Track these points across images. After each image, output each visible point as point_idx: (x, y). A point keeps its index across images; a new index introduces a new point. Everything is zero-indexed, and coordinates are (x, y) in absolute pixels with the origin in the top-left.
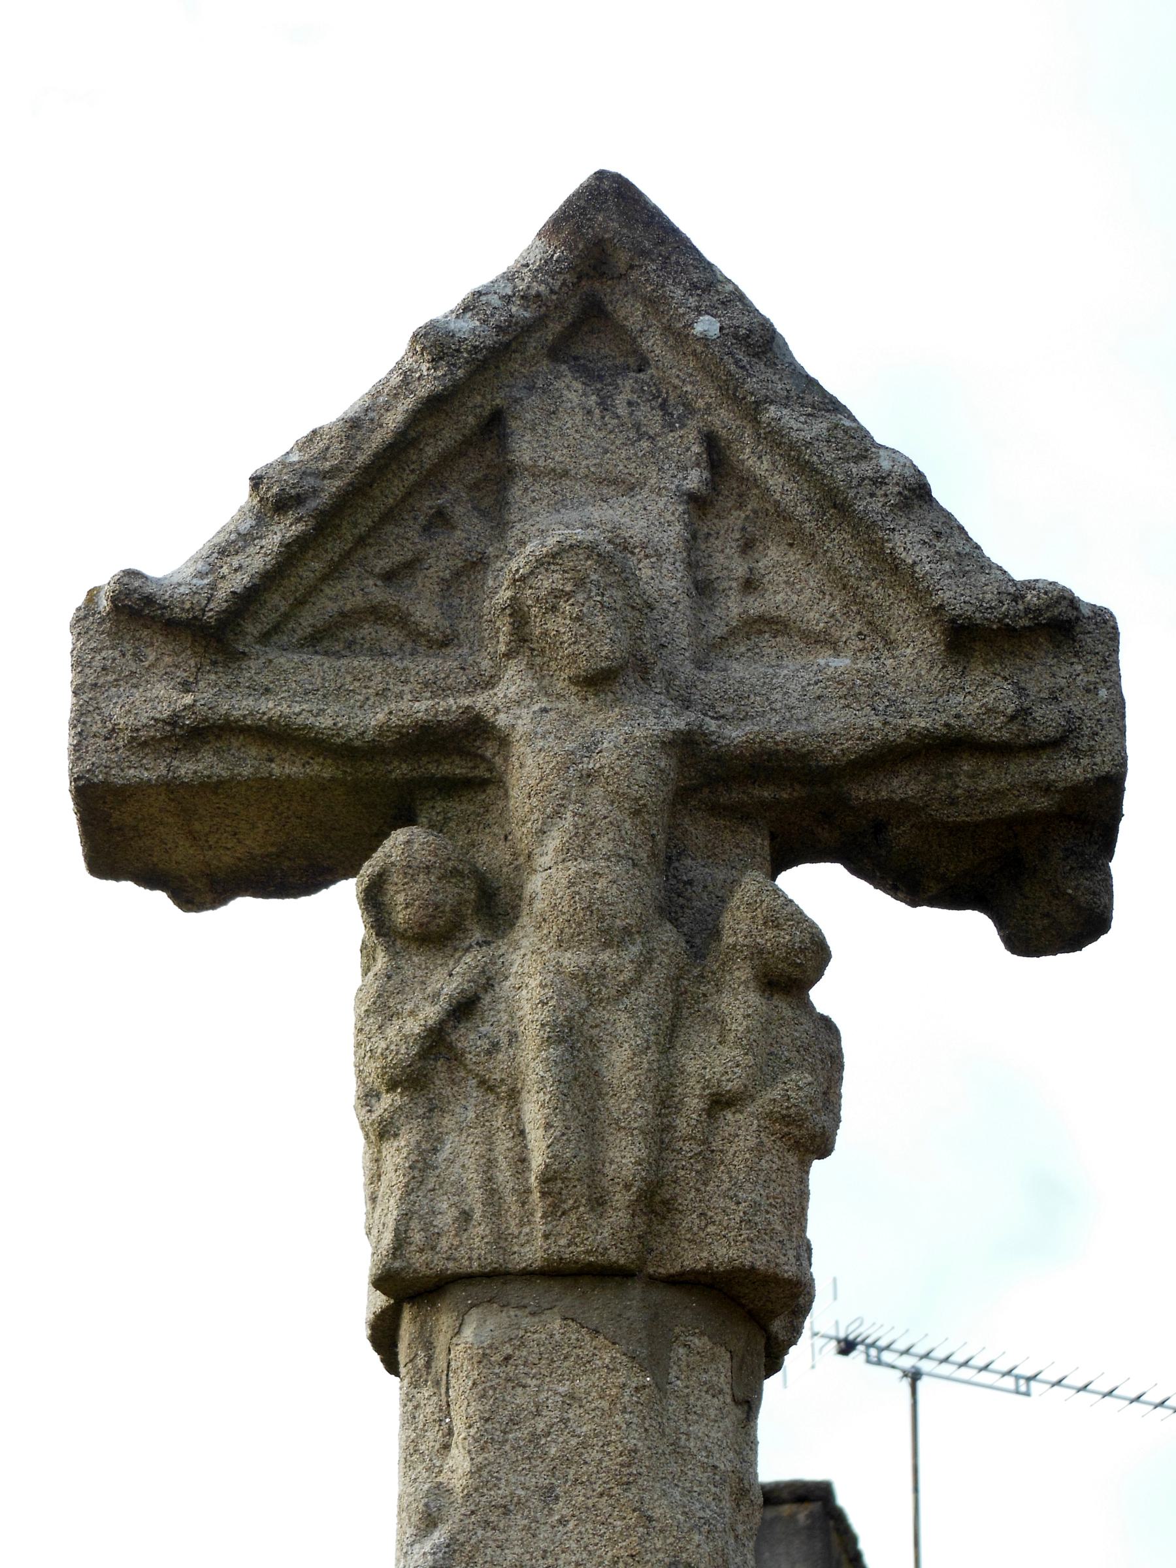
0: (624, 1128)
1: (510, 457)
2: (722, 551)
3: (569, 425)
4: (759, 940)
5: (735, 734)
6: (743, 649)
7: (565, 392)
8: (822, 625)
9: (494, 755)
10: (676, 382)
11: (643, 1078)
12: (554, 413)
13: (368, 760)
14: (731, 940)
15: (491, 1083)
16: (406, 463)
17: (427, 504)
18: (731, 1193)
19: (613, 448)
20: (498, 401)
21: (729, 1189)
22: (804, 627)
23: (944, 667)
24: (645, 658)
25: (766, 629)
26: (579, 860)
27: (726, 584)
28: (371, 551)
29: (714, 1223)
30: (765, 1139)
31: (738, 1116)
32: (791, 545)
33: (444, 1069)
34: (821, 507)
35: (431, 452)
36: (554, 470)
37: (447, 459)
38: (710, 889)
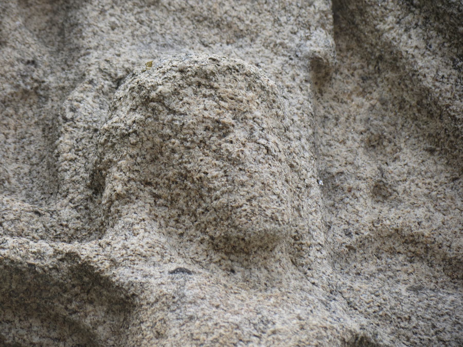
6: (373, 268)
9: (95, 325)
22: (450, 255)
25: (401, 249)
27: (352, 182)
32: (432, 151)
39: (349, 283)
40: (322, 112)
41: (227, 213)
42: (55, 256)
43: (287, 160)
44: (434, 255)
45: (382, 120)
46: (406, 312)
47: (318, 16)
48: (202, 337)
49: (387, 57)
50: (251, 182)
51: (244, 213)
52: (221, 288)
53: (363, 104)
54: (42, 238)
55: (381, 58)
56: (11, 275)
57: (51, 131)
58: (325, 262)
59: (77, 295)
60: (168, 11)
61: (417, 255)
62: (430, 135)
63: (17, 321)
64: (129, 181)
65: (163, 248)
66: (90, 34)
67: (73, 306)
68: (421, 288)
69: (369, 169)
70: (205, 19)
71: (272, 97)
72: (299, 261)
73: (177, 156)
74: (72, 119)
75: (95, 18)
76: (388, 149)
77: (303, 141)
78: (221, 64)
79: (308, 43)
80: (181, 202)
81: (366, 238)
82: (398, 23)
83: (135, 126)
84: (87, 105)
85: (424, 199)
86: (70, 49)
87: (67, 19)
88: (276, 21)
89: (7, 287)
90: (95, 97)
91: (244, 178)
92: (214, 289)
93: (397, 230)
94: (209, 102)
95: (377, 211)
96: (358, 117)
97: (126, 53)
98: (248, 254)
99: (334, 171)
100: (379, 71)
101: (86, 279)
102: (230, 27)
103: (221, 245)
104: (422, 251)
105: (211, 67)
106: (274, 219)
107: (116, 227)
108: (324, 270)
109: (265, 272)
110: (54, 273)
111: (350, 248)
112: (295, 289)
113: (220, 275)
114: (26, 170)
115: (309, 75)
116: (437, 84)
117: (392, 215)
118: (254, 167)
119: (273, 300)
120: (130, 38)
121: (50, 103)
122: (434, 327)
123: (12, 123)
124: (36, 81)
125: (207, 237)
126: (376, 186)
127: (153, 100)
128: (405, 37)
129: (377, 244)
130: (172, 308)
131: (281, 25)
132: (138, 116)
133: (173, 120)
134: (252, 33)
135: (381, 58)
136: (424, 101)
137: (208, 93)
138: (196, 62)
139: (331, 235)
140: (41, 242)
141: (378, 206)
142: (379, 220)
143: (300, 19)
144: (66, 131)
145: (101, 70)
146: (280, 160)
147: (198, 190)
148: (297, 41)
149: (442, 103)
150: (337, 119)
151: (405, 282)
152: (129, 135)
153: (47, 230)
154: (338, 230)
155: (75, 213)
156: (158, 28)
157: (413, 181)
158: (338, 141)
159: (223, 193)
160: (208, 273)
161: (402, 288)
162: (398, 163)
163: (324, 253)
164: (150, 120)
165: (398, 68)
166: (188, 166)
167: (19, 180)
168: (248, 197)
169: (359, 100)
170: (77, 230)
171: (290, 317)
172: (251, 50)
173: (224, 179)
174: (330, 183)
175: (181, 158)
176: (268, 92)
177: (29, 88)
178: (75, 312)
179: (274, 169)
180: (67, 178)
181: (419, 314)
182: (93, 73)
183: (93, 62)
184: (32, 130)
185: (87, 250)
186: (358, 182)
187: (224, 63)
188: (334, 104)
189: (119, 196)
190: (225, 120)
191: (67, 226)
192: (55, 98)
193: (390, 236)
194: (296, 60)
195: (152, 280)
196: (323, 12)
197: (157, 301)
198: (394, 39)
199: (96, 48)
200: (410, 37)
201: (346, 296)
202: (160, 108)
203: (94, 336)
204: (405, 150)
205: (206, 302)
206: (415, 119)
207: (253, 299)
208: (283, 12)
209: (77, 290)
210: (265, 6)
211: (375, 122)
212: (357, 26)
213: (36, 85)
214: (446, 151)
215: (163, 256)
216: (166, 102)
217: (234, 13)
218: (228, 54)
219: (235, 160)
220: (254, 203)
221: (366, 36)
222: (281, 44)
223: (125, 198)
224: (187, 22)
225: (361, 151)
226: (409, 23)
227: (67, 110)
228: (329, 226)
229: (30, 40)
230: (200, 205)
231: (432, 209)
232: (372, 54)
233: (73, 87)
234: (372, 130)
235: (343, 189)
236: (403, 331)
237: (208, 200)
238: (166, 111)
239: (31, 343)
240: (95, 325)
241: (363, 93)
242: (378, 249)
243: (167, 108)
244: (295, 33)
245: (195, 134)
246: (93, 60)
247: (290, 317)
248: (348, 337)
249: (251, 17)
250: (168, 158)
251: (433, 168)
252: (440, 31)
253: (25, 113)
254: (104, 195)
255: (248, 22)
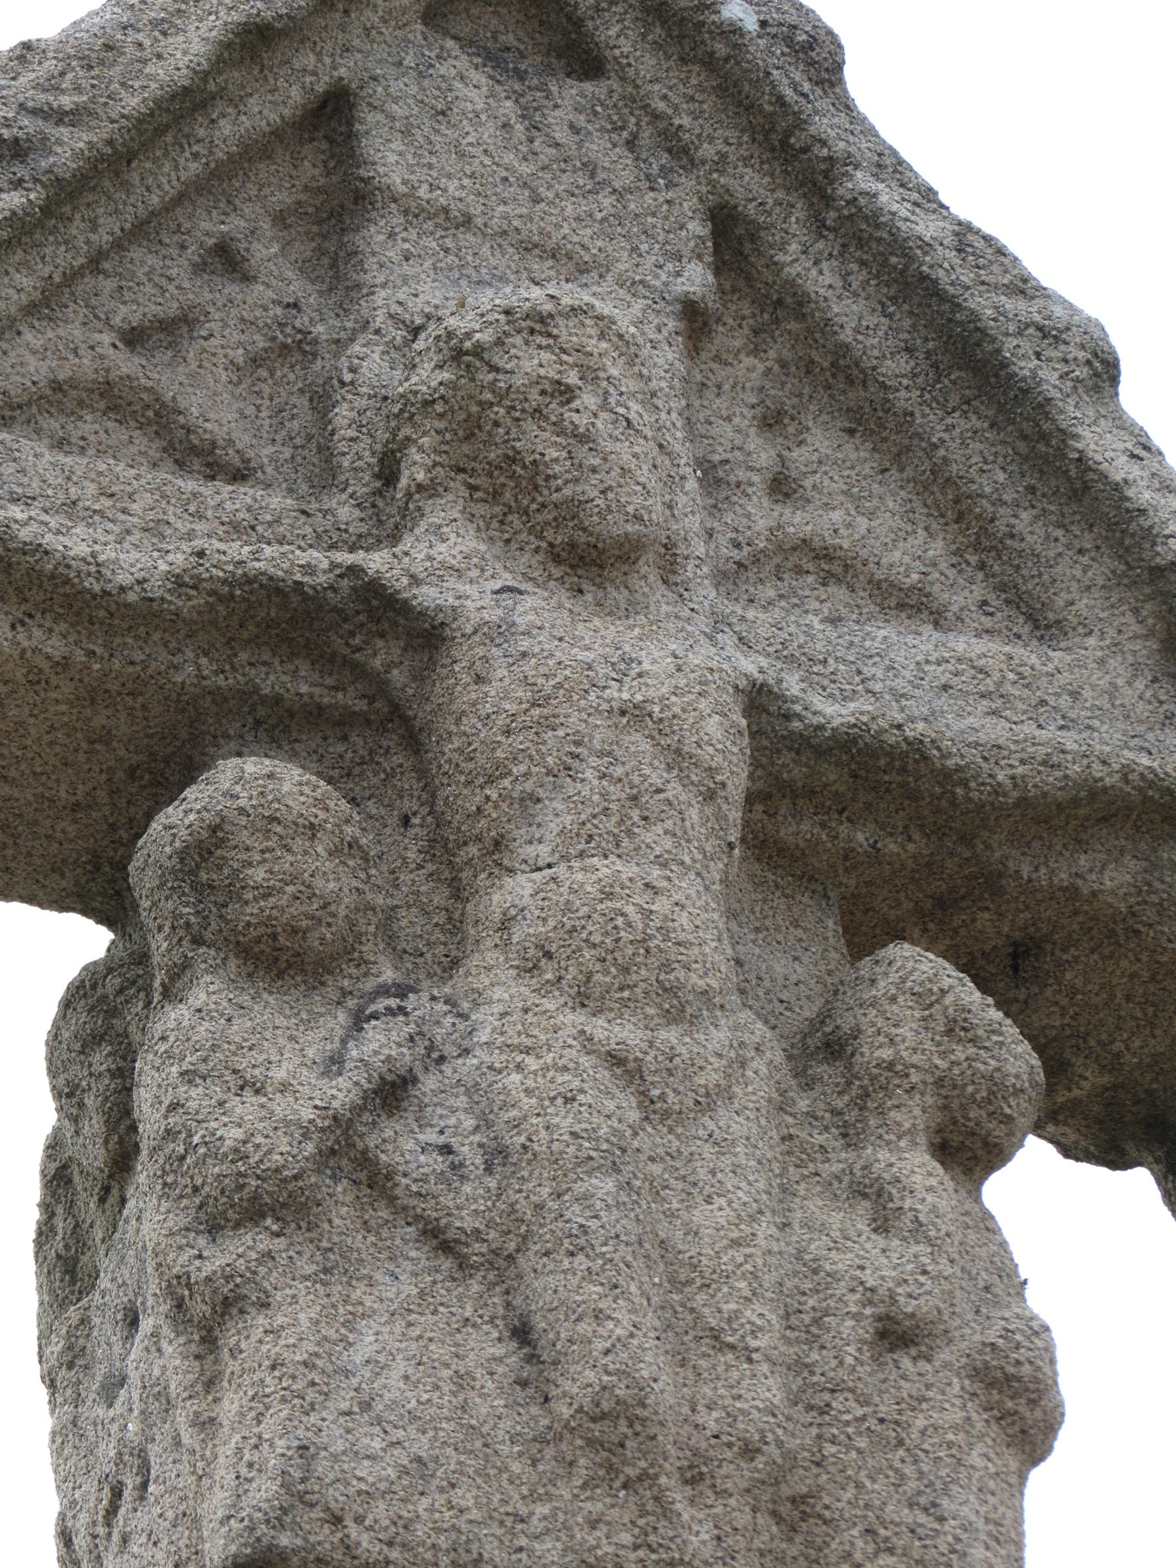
0: (733, 1347)
1: (362, 172)
2: (728, 419)
3: (469, 139)
4: (938, 1062)
5: (834, 712)
6: (772, 593)
7: (458, 85)
8: (915, 577)
9: (388, 667)
10: (661, 106)
11: (760, 1262)
12: (443, 113)
13: (137, 638)
14: (886, 1054)
15: (450, 1235)
16: (187, 136)
17: (210, 225)
18: (923, 1500)
19: (550, 195)
20: (343, 72)
21: (920, 1493)
22: (879, 575)
23: (1155, 680)
24: (675, 545)
25: (810, 567)
26: (612, 858)
27: (741, 474)
28: (108, 285)
29: (891, 1551)
30: (974, 1415)
31: (923, 1365)
32: (851, 432)
33: (348, 1199)
34: (935, 366)
35: (227, 130)
36: (446, 210)
37: (255, 151)
38: (767, 983)
39: (740, 612)
40: (699, 377)
41: (573, 510)
42: (331, 571)
43: (654, 438)
44: (856, 576)
45: (782, 389)
46: (820, 652)
47: (692, 244)
48: (540, 681)
49: (789, 300)
50: (606, 467)
51: (596, 510)
52: (566, 614)
53: (755, 367)
54: (311, 546)
55: (780, 302)
56: (269, 597)
57: (322, 400)
58: (706, 582)
59: (362, 625)
60: (484, 235)
61: (833, 575)
62: (849, 410)
63: (277, 663)
64: (434, 466)
65: (483, 558)
66: (375, 267)
67: (357, 641)
68: (840, 619)
69: (764, 456)
70: (536, 246)
71: (633, 349)
72: (672, 578)
73: (501, 430)
74: (352, 383)
75: (381, 244)
76: (791, 429)
77: (674, 415)
78: (563, 302)
79: (679, 280)
80: (508, 495)
81: (762, 551)
82: (804, 252)
83: (442, 390)
84: (372, 364)
85: (841, 498)
86: (347, 288)
87: (342, 245)
88: (635, 249)
89: (263, 614)
90: (383, 353)
91: (596, 461)
92: (555, 614)
93: (804, 541)
94: (546, 356)
95: (776, 513)
96: (748, 385)
97: (428, 293)
98: (601, 567)
99: (716, 458)
100: (777, 321)
101: (375, 603)
102: (571, 258)
103: (564, 555)
104: (840, 570)
105: (549, 307)
106: (638, 518)
107: (417, 531)
108: (706, 593)
109: (626, 592)
110: (330, 594)
111: (740, 564)
112: (668, 616)
113: (563, 595)
114: (287, 455)
115: (681, 326)
116: (860, 337)
117: (797, 520)
118: (609, 446)
119: (637, 631)
120: (431, 272)
121: (319, 362)
122: (859, 672)
123: (267, 390)
124: (300, 331)
125: (544, 545)
126: (775, 480)
127: (467, 353)
128: (814, 272)
129: (777, 560)
130: (497, 641)
131: (640, 256)
132: (446, 375)
133: (496, 380)
134: (601, 266)
135: (780, 302)
136: (841, 362)
137: (544, 343)
138: (527, 299)
139: (713, 546)
140: (310, 551)
141: (778, 508)
142: (779, 527)
143: (668, 247)
144: (344, 399)
145: (391, 316)
146: (645, 437)
147: (532, 479)
148: (664, 277)
149: (866, 363)
150: (719, 387)
151: (816, 612)
152: (434, 401)
153: (319, 537)
154: (723, 540)
155: (357, 513)
156: (470, 258)
157: (826, 473)
158: (721, 417)
159: (567, 482)
160: (546, 594)
161: (816, 621)
162: (804, 448)
163: (705, 569)
164: (463, 381)
165: (804, 315)
166: (518, 444)
167: (277, 469)
168: (601, 487)
169: (749, 361)
170: (360, 536)
171: (662, 653)
172: (599, 290)
173: (568, 463)
174: (712, 476)
175: (507, 433)
176: (628, 342)
177: (289, 341)
178: (360, 649)
179: (637, 449)
180: (346, 464)
181: (839, 654)
182: (379, 320)
183: (381, 303)
184: (294, 400)
185: (376, 562)
186: (749, 473)
187: (566, 301)
188: (715, 366)
189: (420, 487)
190: (569, 381)
191: (346, 531)
192: (327, 356)
193: (794, 549)
194: (663, 304)
195: (469, 603)
196: (700, 237)
197: (475, 632)
198: (798, 275)
199: (384, 285)
200: (821, 272)
201: (737, 629)
202: (478, 364)
203: (387, 682)
204: (813, 431)
205: (545, 633)
206: (828, 387)
207: (611, 630)
208: (643, 237)
209: (362, 618)
210: (619, 229)
211: (772, 392)
212: (746, 258)
213: (299, 336)
214: (872, 432)
215: (483, 570)
216: (486, 356)
217: (576, 239)
218: (571, 295)
219: (583, 435)
220: (610, 495)
221: (758, 272)
222: (641, 282)
223: (429, 489)
224: (511, 250)
225: (753, 430)
226: (820, 253)
227: (345, 371)
228: (710, 534)
229: (290, 274)
230: (533, 500)
231: (853, 512)
232: (767, 296)
233: (352, 340)
234: (768, 403)
235: (728, 484)
236: (816, 678)
237: (546, 492)
238: (486, 368)
239: (297, 694)
240: (388, 667)
241: (755, 352)
242: (778, 566)
243: (487, 364)
244: (660, 267)
245: (526, 400)
246: (380, 303)
247: (662, 653)
248: (743, 683)
249: (599, 244)
250: (489, 433)
251: (853, 456)
252: (863, 263)
253: (284, 376)
254: (400, 486)
255: (594, 251)
